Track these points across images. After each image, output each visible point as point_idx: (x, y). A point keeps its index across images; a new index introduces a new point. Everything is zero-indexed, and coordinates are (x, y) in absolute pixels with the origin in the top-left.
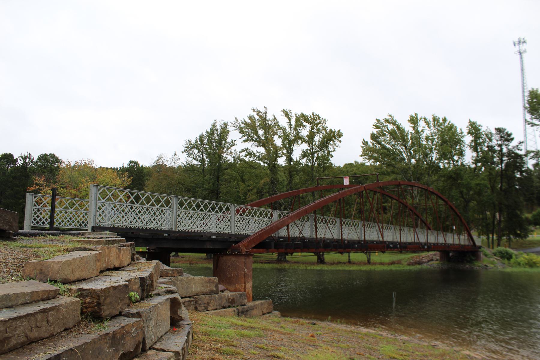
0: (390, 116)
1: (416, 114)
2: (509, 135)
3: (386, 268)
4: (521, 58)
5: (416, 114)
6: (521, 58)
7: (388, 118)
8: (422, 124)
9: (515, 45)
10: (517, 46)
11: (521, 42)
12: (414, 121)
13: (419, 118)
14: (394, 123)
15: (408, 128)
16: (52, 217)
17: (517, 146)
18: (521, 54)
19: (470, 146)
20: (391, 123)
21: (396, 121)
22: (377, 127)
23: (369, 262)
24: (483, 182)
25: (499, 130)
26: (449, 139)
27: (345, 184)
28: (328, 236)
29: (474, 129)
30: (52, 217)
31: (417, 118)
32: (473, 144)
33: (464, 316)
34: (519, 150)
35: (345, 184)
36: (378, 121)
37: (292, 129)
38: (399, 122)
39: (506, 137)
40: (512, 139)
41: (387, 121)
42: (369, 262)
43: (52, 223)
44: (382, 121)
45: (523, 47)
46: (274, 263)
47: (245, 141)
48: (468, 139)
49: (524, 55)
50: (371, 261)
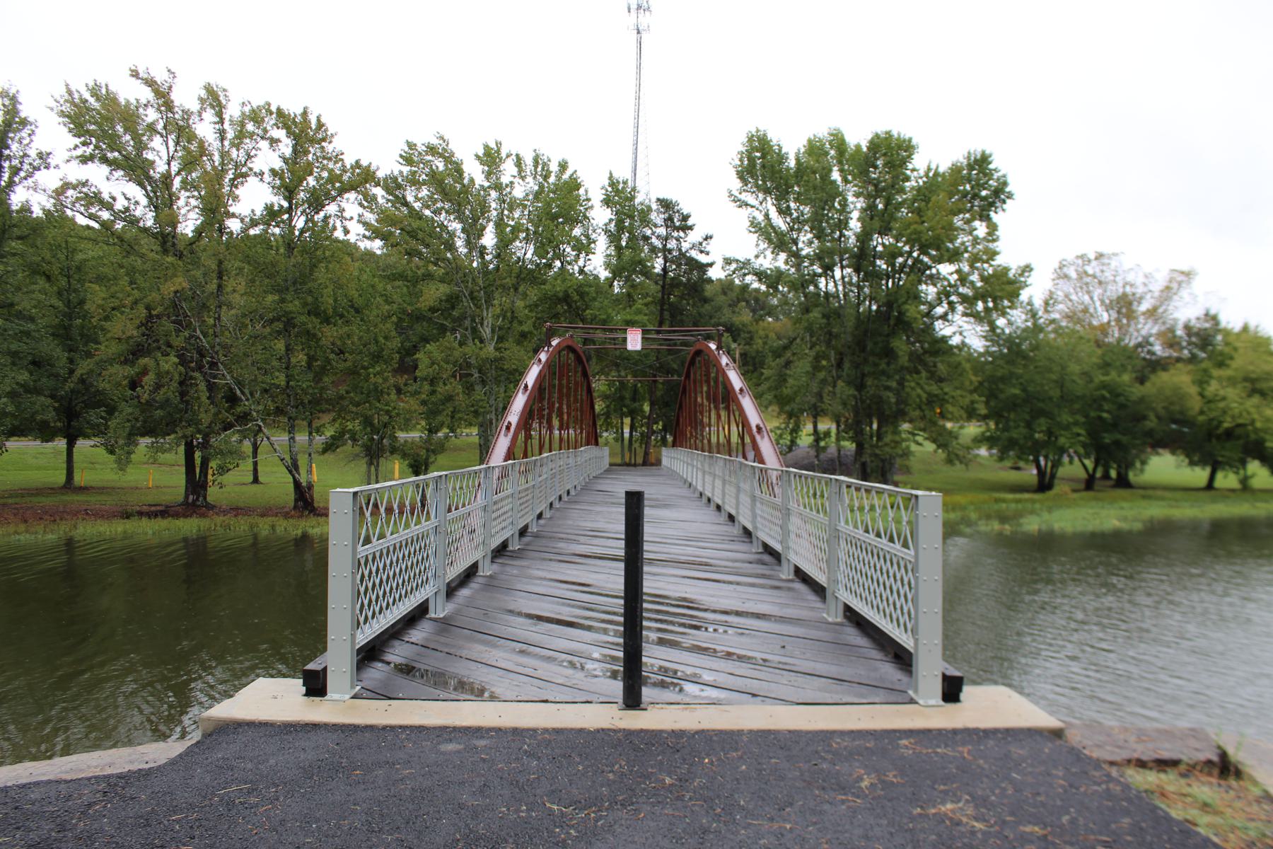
0: (442, 138)
2: (685, 218)
5: (499, 144)
7: (435, 142)
8: (508, 171)
12: (491, 158)
13: (503, 155)
14: (448, 158)
15: (474, 172)
17: (701, 244)
19: (606, 231)
20: (441, 155)
21: (452, 154)
22: (408, 160)
25: (666, 205)
26: (559, 206)
27: (630, 347)
29: (619, 196)
31: (498, 151)
32: (612, 227)
34: (702, 252)
35: (630, 347)
36: (411, 145)
37: (226, 143)
38: (458, 156)
39: (677, 221)
40: (691, 228)
41: (432, 150)
44: (421, 148)
45: (645, 19)
46: (176, 515)
47: (84, 160)
48: (601, 216)
49: (644, 35)
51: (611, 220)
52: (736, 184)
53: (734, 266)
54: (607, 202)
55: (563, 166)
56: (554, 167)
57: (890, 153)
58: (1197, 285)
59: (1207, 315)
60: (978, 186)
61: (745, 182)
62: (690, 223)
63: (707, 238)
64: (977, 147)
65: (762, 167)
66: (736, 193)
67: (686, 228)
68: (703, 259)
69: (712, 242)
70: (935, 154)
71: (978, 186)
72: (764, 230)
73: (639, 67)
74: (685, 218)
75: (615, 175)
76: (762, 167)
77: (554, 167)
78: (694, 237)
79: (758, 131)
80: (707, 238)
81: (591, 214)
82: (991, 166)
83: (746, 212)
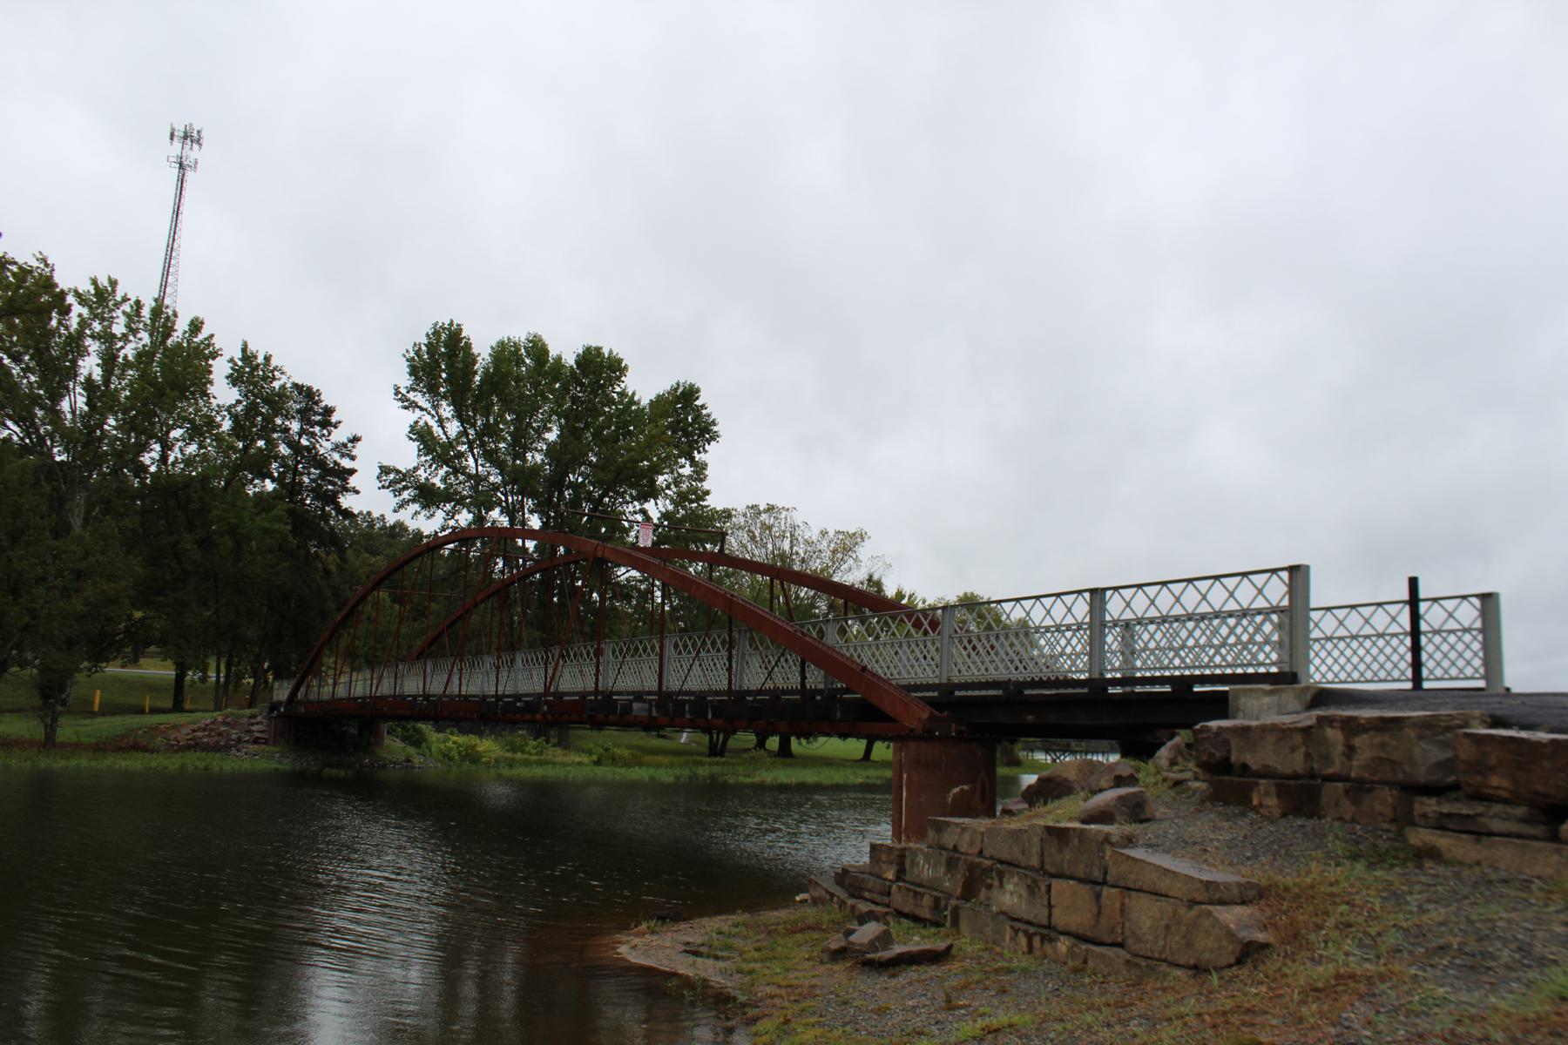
0: (44, 261)
1: (113, 283)
3: (173, 763)
4: (181, 180)
5: (113, 283)
6: (181, 180)
9: (172, 136)
10: (177, 144)
11: (190, 137)
16: (1417, 665)
18: (181, 166)
23: (49, 743)
24: (277, 526)
26: (175, 368)
28: (696, 683)
30: (1417, 665)
33: (287, 894)
42: (49, 743)
43: (1417, 678)
45: (193, 154)
49: (189, 174)
50: (58, 740)
51: (239, 402)
52: (405, 381)
53: (392, 476)
54: (235, 379)
55: (196, 326)
56: (182, 326)
57: (599, 369)
58: (863, 551)
59: (870, 579)
60: (683, 422)
61: (418, 379)
62: (334, 419)
63: (355, 439)
64: (686, 377)
65: (442, 364)
66: (404, 391)
67: (326, 424)
68: (346, 463)
69: (359, 445)
70: (644, 384)
71: (683, 422)
72: (421, 435)
73: (177, 212)
74: (329, 411)
75: (252, 347)
76: (442, 364)
77: (182, 326)
78: (339, 436)
79: (451, 324)
80: (355, 439)
81: (211, 390)
82: (698, 403)
83: (412, 416)
